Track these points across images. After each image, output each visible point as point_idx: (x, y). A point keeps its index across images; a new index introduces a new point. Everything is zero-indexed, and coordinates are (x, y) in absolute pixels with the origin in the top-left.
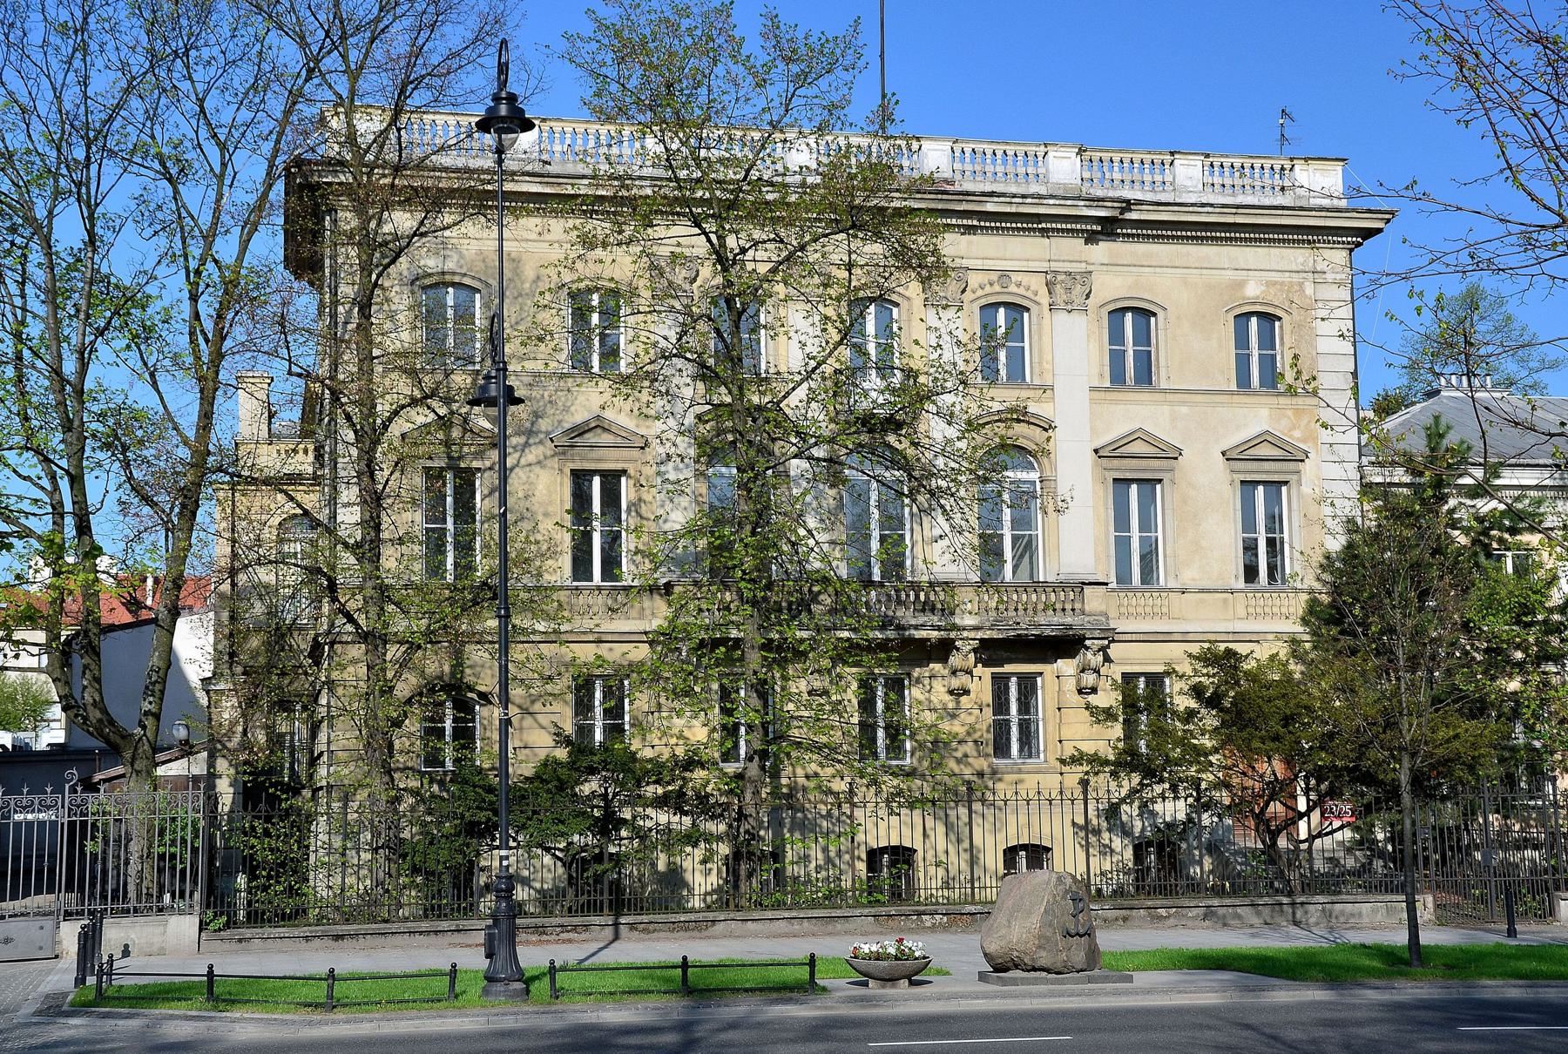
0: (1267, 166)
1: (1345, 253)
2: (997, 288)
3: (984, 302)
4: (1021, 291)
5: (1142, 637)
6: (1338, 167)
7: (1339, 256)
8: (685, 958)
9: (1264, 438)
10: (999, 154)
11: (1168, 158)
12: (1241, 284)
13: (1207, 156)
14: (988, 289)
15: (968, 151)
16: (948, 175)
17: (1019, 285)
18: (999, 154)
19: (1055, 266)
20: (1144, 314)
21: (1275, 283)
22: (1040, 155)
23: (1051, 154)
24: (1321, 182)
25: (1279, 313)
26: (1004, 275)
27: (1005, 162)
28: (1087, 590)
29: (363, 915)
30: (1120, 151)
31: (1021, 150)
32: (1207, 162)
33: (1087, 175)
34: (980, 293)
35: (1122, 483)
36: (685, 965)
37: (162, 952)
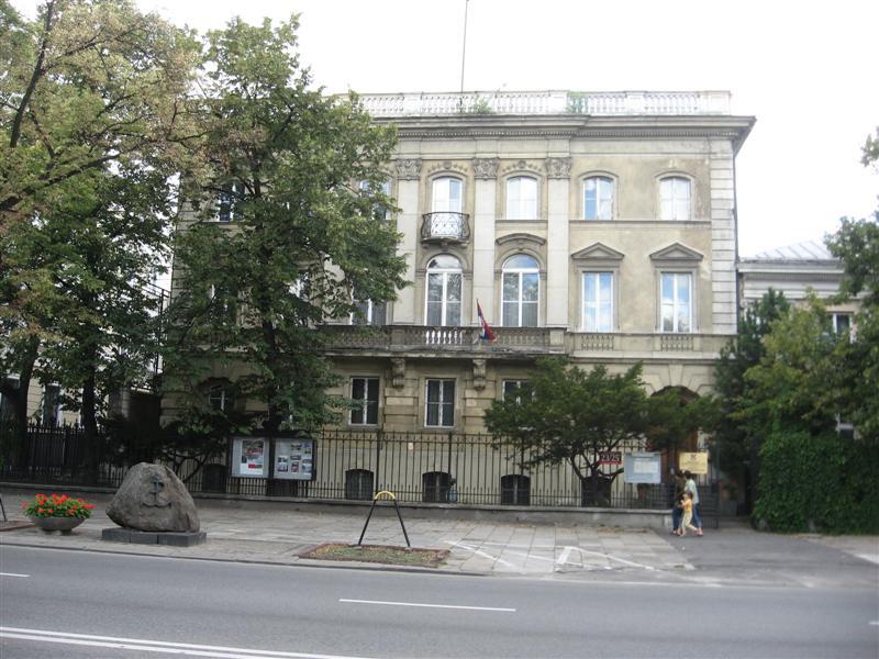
2: (518, 169)
4: (532, 169)
14: (513, 169)
17: (530, 166)
26: (522, 161)
28: (552, 333)
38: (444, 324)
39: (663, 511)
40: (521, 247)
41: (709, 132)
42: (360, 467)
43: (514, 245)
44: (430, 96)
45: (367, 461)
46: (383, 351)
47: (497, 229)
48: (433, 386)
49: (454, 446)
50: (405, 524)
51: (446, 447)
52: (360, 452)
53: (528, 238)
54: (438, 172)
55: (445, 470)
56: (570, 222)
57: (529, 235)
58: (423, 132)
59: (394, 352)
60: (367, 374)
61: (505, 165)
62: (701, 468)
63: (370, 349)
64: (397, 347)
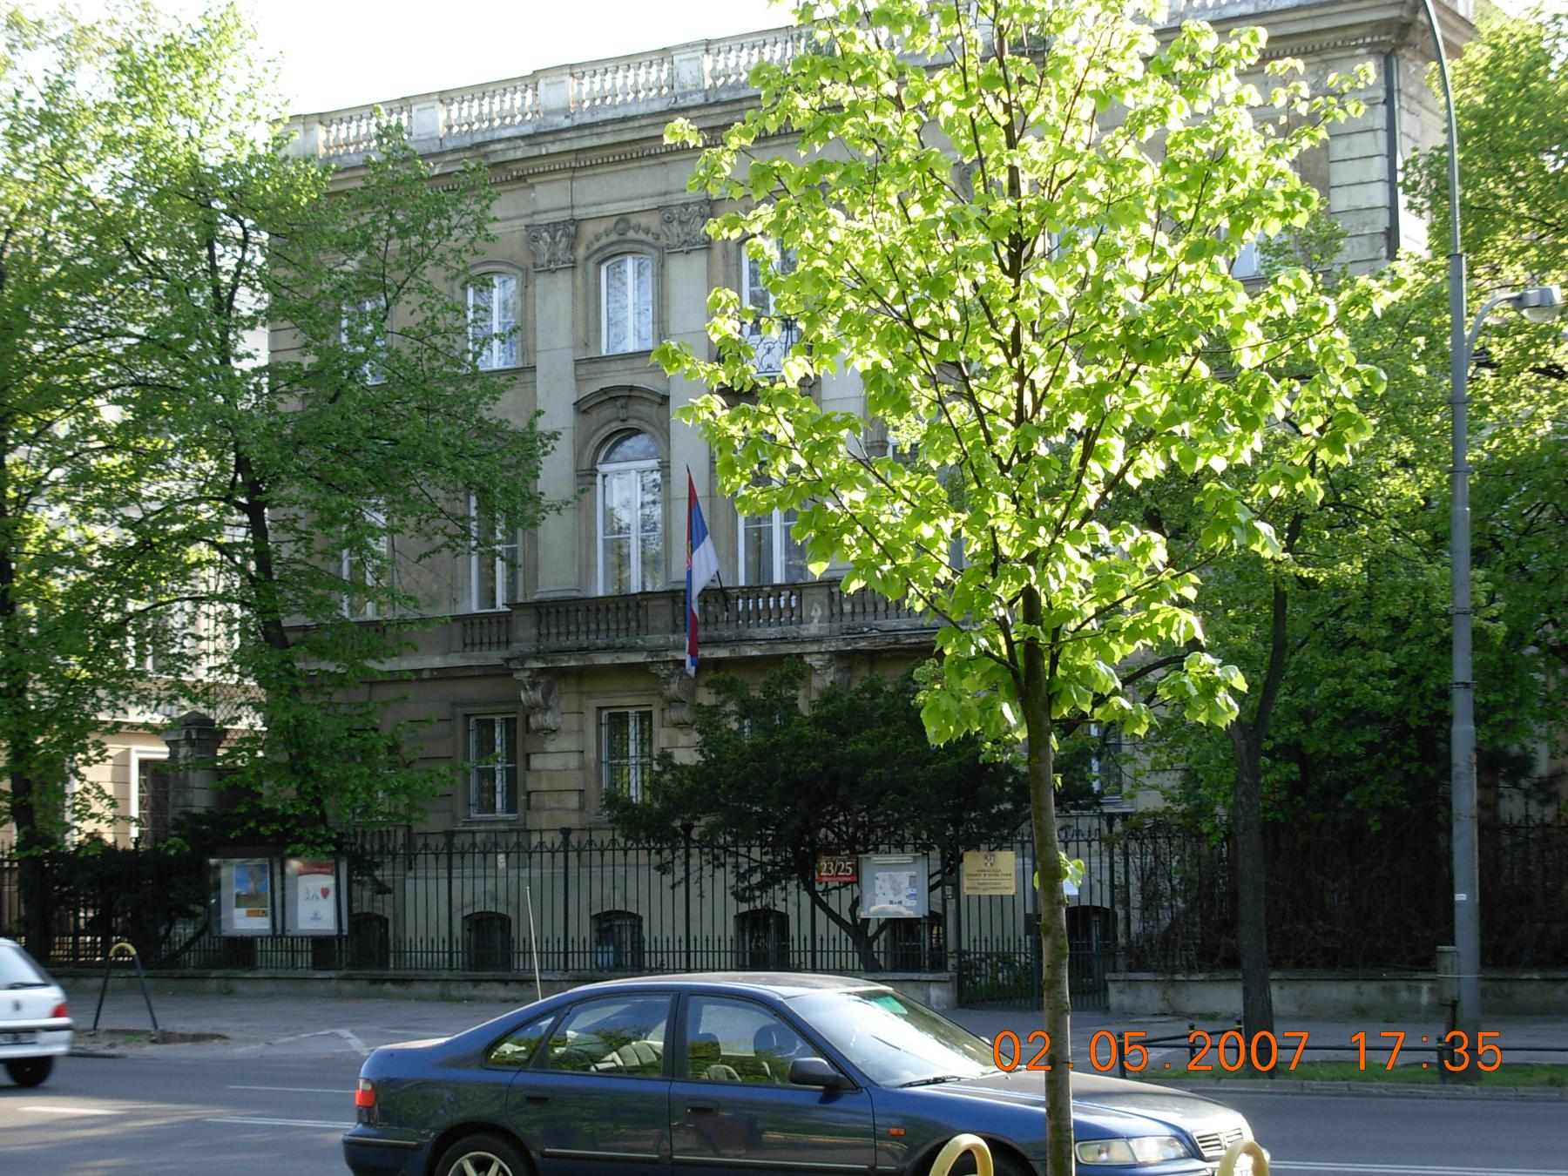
38: (778, 578)
39: (924, 976)
40: (622, 414)
41: (1316, 41)
42: (619, 906)
43: (607, 412)
44: (724, 47)
45: (632, 893)
46: (634, 649)
47: (578, 380)
48: (618, 721)
49: (573, 856)
50: (157, 1014)
51: (560, 857)
52: (620, 871)
53: (630, 395)
54: (601, 249)
55: (1107, 905)
56: (577, 362)
57: (631, 388)
58: (569, 161)
59: (651, 651)
60: (627, 700)
61: (589, 230)
62: (1004, 884)
63: (606, 649)
64: (657, 639)
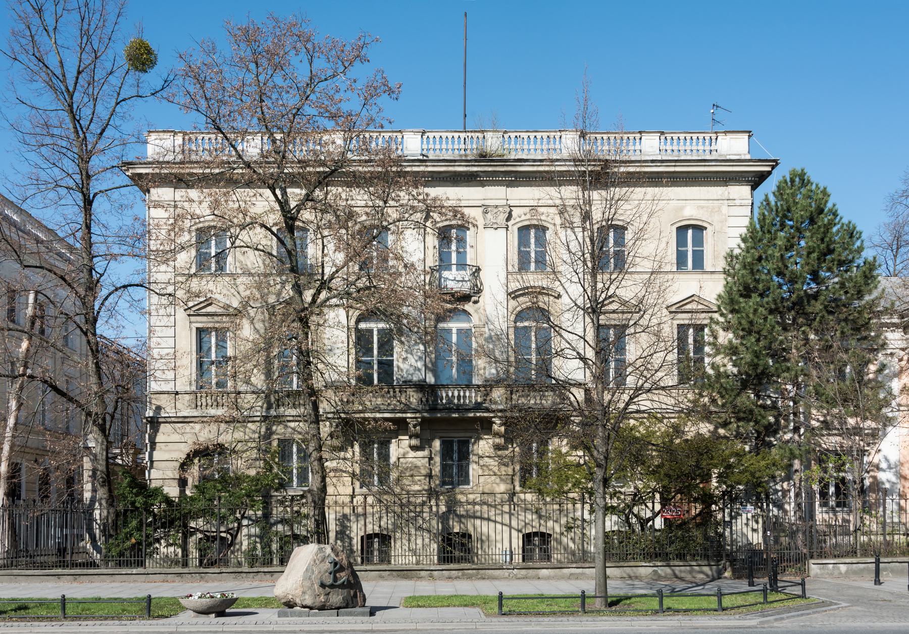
0: (688, 137)
1: (748, 188)
3: (520, 225)
5: (180, 420)
6: (746, 136)
7: (746, 189)
8: (583, 592)
9: (691, 299)
10: (532, 137)
11: (714, 136)
12: (682, 208)
13: (505, 132)
14: (523, 217)
15: (545, 137)
16: (500, 152)
18: (532, 137)
19: (487, 203)
20: (699, 229)
21: (702, 207)
22: (557, 138)
23: (564, 137)
24: (733, 146)
25: (705, 224)
27: (535, 143)
29: (277, 566)
30: (608, 133)
31: (437, 135)
32: (663, 138)
33: (663, 147)
34: (518, 220)
35: (200, 331)
36: (64, 599)
37: (135, 581)
